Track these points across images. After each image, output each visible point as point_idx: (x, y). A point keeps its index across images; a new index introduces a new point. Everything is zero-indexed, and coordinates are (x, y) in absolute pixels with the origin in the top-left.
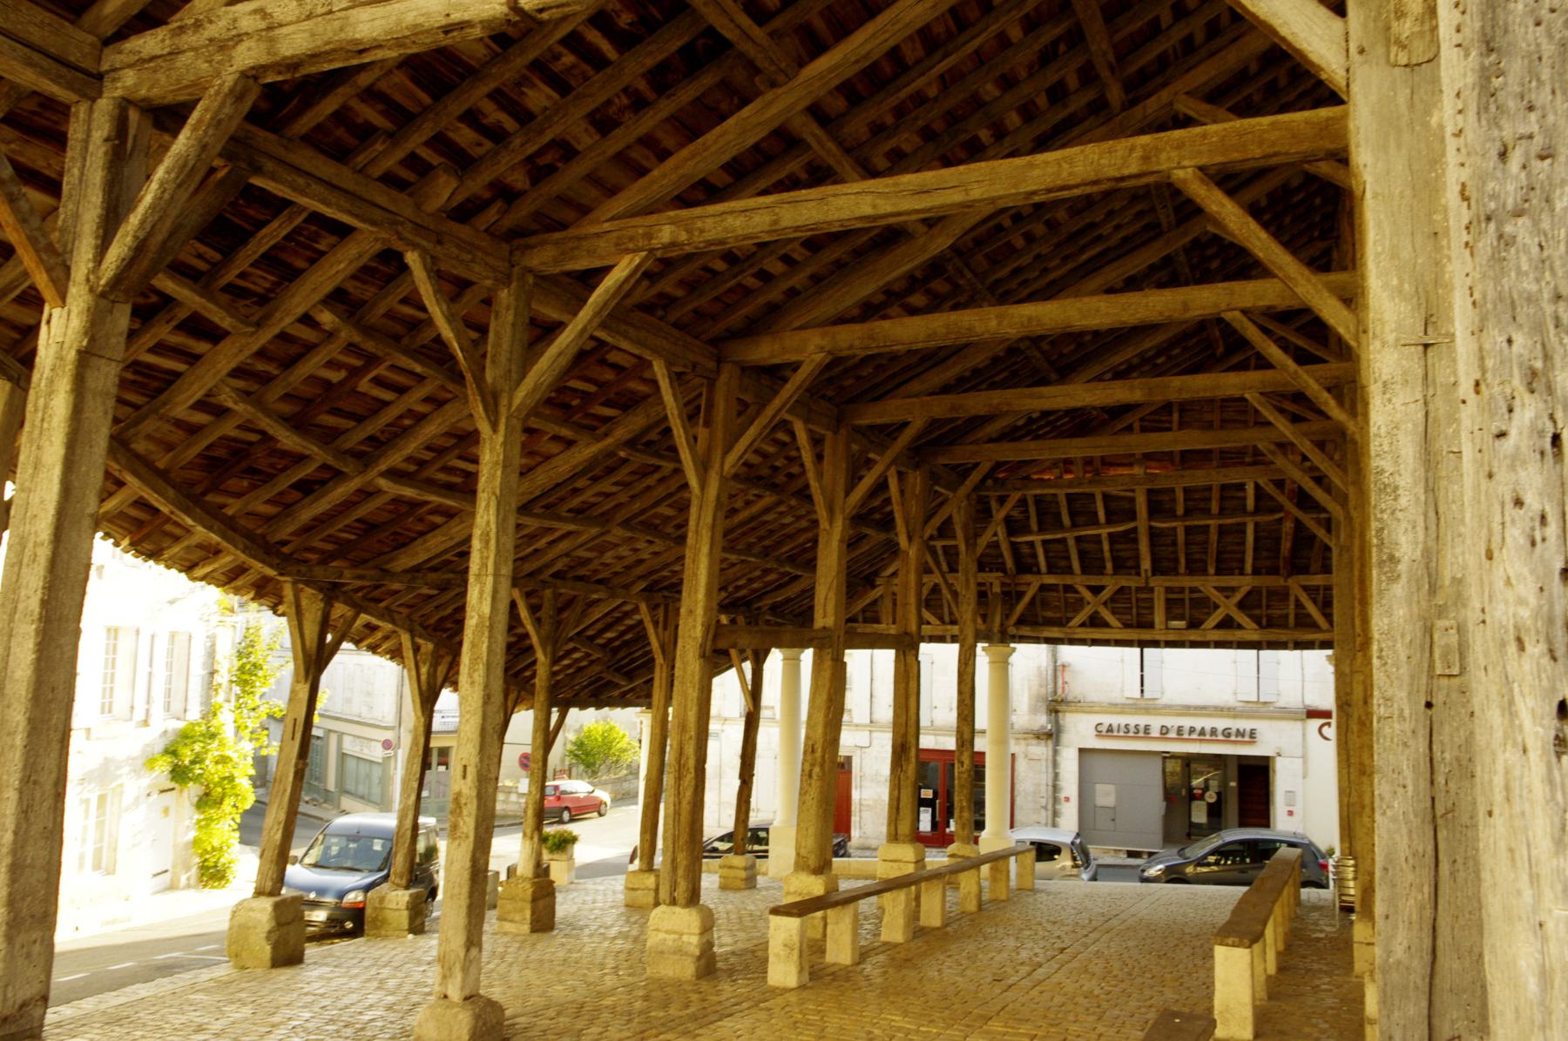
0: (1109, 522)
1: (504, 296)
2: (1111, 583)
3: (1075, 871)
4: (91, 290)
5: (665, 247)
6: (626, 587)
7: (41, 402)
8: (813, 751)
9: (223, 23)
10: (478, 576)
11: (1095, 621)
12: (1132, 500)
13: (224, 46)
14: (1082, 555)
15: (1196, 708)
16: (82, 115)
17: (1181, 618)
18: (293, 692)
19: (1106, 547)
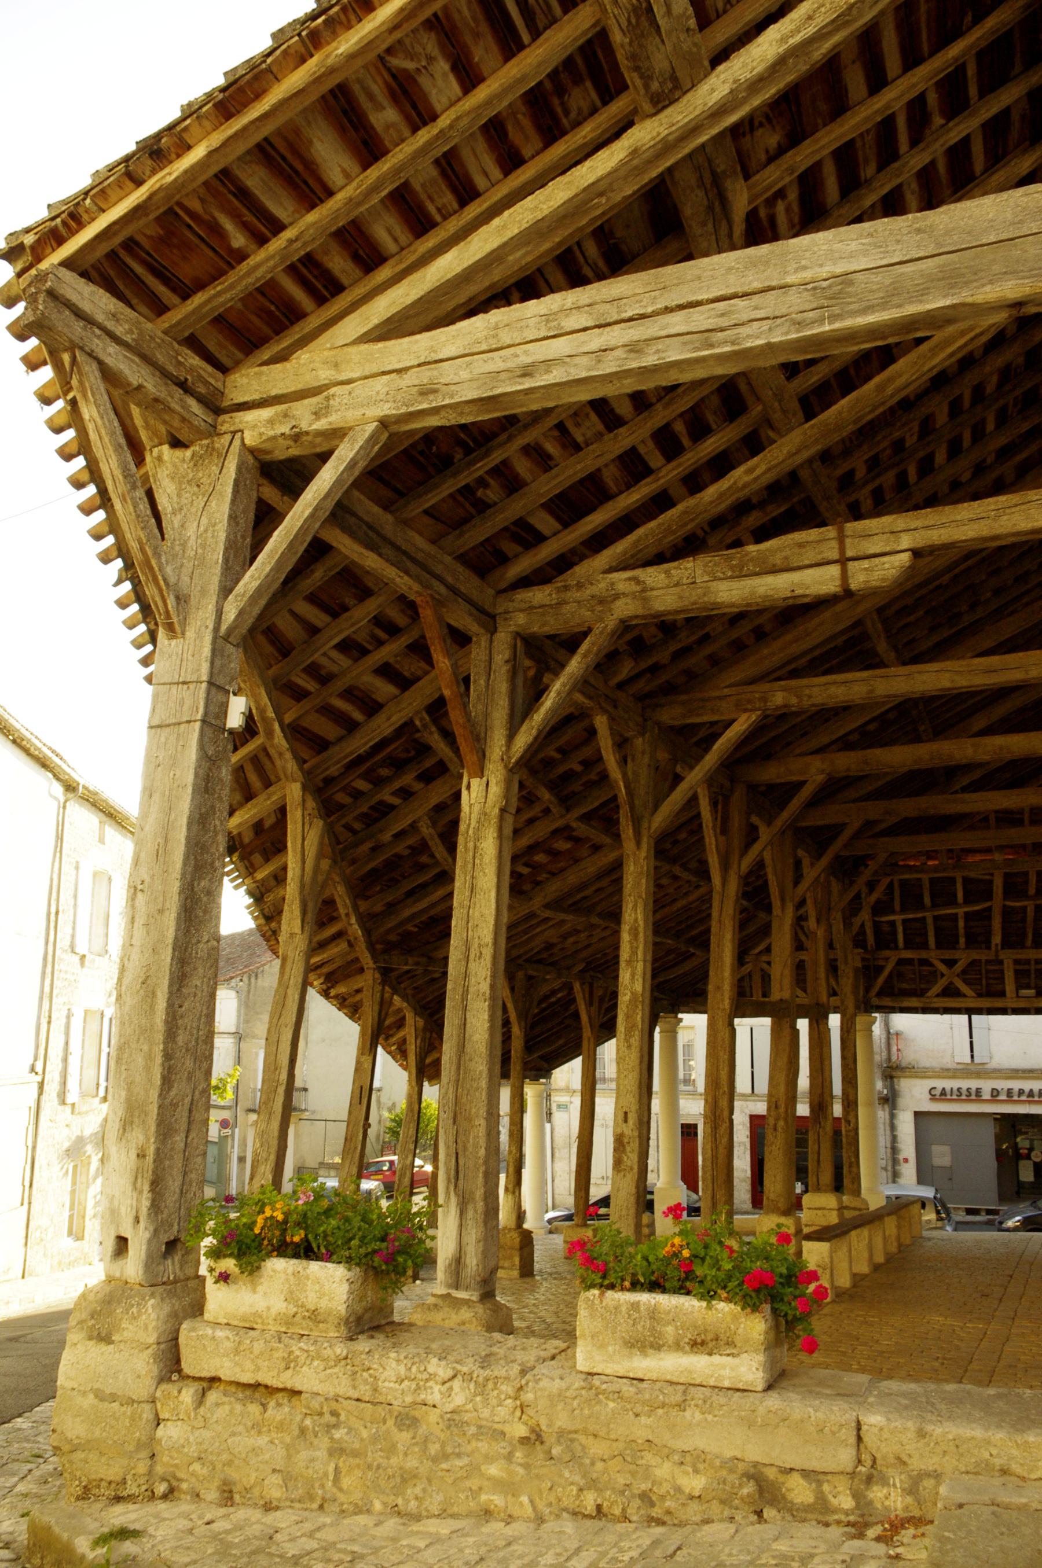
0: (967, 901)
1: (639, 742)
2: (964, 957)
3: (939, 1224)
4: (506, 766)
5: (778, 708)
6: (568, 968)
7: (471, 845)
8: (777, 1107)
9: (602, 585)
10: (629, 962)
11: (950, 992)
12: (991, 882)
13: (604, 601)
14: (938, 931)
15: (1024, 1071)
16: (483, 644)
17: (1028, 987)
18: (358, 1063)
19: (961, 924)
